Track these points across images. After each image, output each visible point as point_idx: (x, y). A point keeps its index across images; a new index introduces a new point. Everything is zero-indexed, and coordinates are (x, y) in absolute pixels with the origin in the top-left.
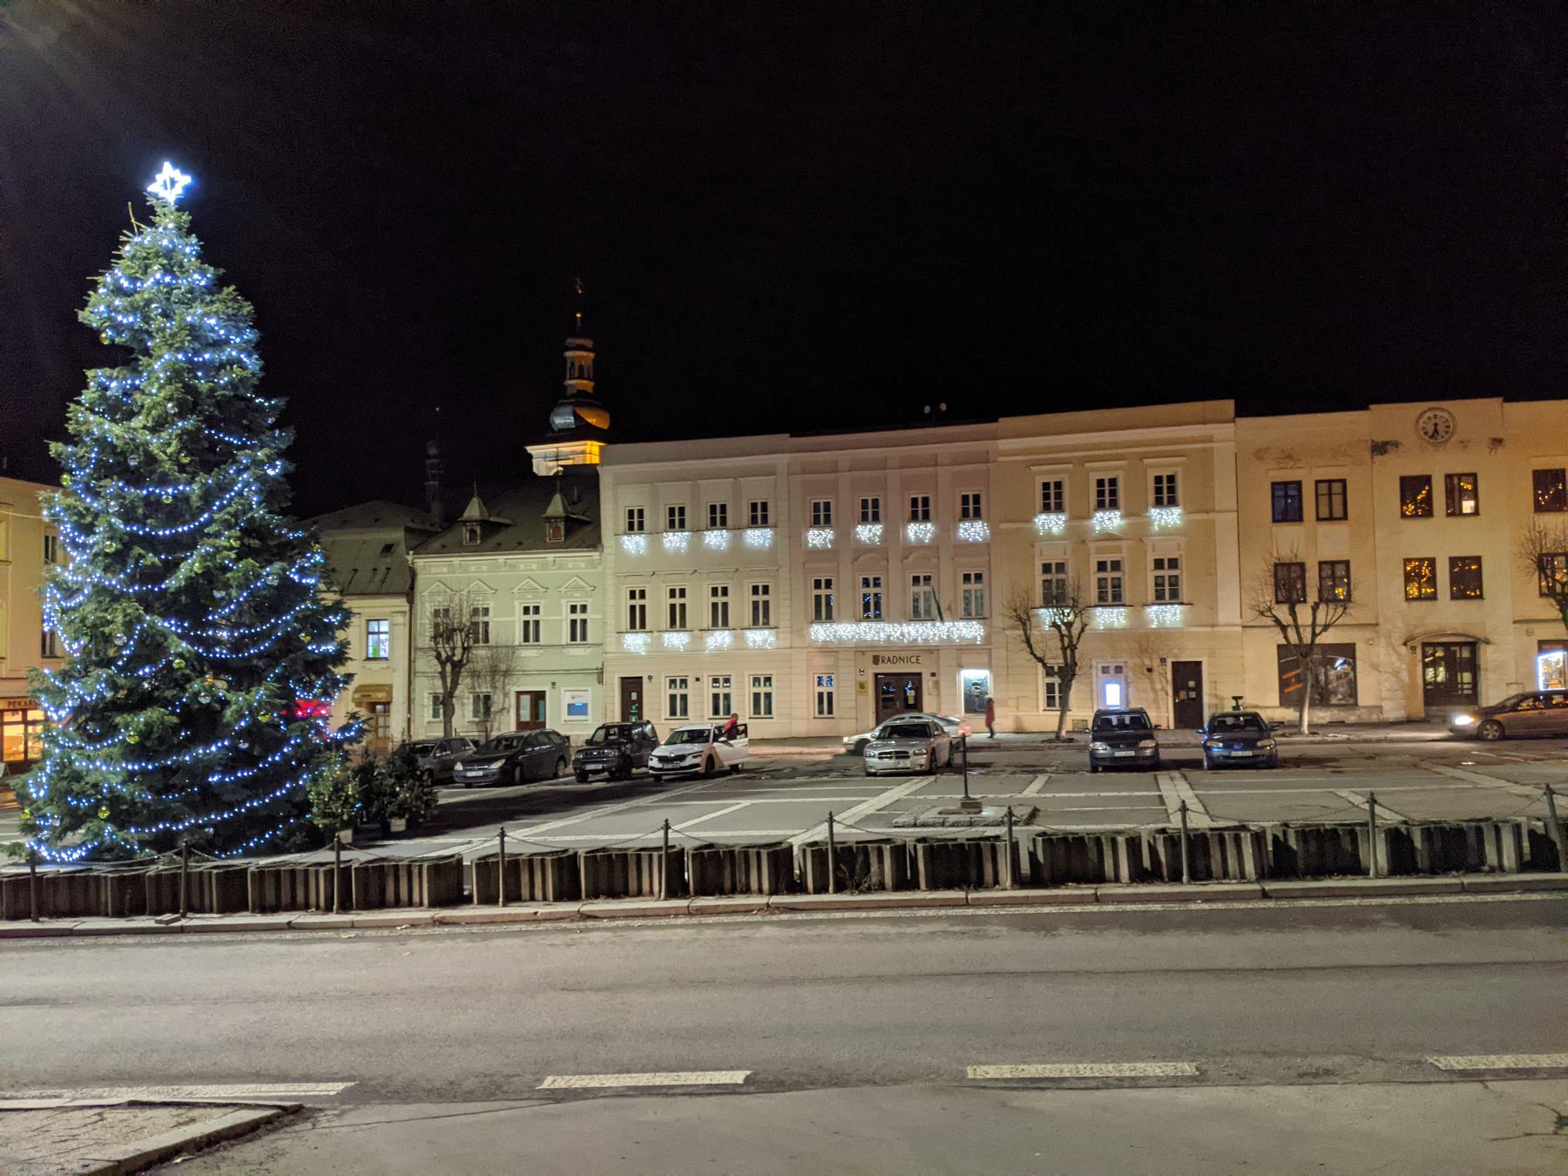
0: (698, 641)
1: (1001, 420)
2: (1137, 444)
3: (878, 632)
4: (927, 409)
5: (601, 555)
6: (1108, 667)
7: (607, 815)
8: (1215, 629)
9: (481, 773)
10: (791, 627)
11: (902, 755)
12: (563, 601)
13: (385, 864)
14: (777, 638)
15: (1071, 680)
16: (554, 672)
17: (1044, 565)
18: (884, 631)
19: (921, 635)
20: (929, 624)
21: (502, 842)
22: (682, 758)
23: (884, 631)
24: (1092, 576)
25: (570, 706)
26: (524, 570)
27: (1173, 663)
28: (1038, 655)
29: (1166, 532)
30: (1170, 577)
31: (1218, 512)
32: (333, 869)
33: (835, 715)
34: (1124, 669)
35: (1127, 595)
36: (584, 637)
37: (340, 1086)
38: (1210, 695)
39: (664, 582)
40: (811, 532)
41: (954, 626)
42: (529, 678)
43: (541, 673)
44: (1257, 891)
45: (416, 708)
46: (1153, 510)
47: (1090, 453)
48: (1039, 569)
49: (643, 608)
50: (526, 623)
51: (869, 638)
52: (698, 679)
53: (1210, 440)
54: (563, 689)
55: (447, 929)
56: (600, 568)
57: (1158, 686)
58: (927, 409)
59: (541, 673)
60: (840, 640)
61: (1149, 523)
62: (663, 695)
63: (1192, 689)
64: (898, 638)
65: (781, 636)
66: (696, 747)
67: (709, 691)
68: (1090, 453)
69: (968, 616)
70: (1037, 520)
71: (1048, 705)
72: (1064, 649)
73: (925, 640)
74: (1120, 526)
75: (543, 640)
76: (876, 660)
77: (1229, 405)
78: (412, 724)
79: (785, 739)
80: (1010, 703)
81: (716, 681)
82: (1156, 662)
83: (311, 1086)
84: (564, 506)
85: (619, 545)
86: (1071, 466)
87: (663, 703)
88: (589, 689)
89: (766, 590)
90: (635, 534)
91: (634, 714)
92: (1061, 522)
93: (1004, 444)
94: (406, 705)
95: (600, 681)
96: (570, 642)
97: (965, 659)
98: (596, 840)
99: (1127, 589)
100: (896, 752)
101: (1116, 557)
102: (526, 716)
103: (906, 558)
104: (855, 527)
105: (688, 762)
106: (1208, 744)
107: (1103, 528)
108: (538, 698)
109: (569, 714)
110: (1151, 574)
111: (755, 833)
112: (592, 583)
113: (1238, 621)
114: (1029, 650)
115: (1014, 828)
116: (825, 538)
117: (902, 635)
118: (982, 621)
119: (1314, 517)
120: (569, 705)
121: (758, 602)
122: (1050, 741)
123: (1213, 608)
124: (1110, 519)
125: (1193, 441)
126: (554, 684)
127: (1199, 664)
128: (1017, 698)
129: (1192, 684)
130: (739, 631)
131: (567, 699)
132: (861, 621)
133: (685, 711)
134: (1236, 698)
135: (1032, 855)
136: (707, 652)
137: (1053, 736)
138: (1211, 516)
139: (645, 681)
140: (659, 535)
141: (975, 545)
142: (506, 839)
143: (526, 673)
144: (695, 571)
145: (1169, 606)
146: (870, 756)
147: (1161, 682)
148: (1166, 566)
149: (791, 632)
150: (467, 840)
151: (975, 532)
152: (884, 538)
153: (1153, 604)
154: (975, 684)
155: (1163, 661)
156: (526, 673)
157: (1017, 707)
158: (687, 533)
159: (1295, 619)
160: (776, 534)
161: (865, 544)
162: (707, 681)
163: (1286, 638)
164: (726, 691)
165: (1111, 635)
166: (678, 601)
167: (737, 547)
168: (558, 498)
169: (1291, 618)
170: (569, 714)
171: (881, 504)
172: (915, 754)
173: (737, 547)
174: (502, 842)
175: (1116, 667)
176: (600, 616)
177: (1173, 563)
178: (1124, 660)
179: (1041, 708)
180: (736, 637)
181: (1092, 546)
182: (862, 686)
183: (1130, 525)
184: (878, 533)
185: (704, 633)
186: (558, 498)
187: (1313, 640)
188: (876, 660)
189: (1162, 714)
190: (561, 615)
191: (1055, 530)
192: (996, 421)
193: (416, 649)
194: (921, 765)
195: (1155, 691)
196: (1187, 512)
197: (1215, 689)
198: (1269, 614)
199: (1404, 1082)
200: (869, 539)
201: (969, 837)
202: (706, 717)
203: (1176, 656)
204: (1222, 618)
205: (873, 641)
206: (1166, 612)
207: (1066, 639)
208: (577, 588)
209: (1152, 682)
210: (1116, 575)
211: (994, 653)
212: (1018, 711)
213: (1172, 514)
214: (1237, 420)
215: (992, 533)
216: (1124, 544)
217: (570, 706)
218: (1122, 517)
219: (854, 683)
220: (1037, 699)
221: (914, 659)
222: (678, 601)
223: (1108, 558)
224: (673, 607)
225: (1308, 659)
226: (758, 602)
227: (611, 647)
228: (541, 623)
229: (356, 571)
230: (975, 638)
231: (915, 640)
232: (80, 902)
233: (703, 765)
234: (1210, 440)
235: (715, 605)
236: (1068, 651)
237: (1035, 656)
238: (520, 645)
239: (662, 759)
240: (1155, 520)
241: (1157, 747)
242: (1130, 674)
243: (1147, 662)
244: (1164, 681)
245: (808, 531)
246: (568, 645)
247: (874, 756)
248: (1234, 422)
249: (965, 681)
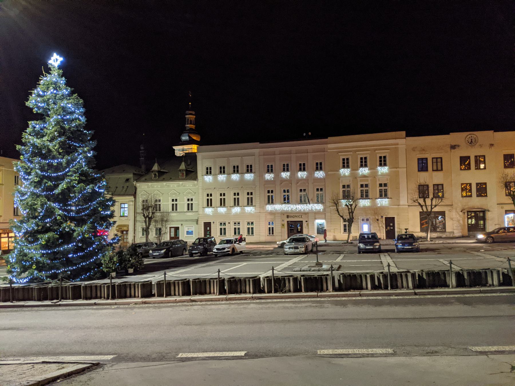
0: (229, 210)
1: (329, 138)
2: (374, 146)
3: (288, 208)
4: (305, 134)
5: (197, 182)
6: (364, 219)
7: (199, 267)
8: (399, 206)
9: (158, 254)
10: (260, 206)
11: (296, 248)
12: (185, 197)
13: (127, 283)
14: (255, 209)
15: (352, 223)
16: (182, 221)
17: (343, 185)
18: (290, 207)
19: (303, 209)
20: (305, 205)
21: (165, 276)
22: (224, 249)
23: (290, 207)
24: (359, 189)
25: (187, 232)
26: (172, 187)
27: (385, 218)
28: (341, 215)
29: (383, 175)
30: (384, 189)
31: (400, 168)
32: (109, 285)
33: (274, 235)
34: (369, 220)
35: (370, 195)
36: (192, 209)
37: (112, 357)
38: (397, 228)
40: (266, 175)
41: (313, 205)
42: (174, 223)
43: (178, 221)
44: (413, 292)
45: (137, 232)
46: (379, 167)
47: (358, 149)
48: (341, 187)
49: (211, 199)
50: (173, 205)
51: (285, 209)
52: (229, 223)
53: (398, 144)
54: (185, 226)
55: (147, 305)
56: (197, 186)
57: (380, 225)
58: (305, 134)
59: (178, 221)
60: (276, 210)
61: (377, 172)
62: (218, 228)
63: (392, 226)
64: (295, 209)
65: (257, 209)
66: (229, 245)
67: (233, 227)
68: (358, 149)
69: (318, 202)
70: (340, 171)
71: (344, 232)
72: (349, 213)
73: (304, 210)
74: (368, 173)
75: (178, 210)
76: (288, 217)
77: (404, 133)
78: (135, 238)
79: (258, 243)
80: (332, 231)
81: (235, 223)
82: (380, 217)
84: (185, 166)
85: (203, 179)
86: (352, 153)
87: (218, 231)
88: (194, 226)
89: (252, 194)
90: (209, 175)
91: (208, 234)
92: (348, 171)
93: (330, 146)
94: (133, 231)
95: (197, 224)
96: (187, 211)
97: (317, 216)
98: (196, 276)
99: (370, 193)
100: (294, 247)
101: (366, 183)
102: (173, 235)
103: (298, 183)
104: (281, 173)
105: (226, 250)
106: (397, 244)
107: (362, 173)
108: (177, 229)
109: (187, 234)
110: (378, 188)
111: (248, 273)
112: (195, 191)
113: (407, 204)
114: (338, 213)
115: (333, 272)
117: (296, 208)
118: (322, 204)
119: (432, 170)
120: (187, 232)
122: (345, 243)
123: (398, 200)
124: (364, 170)
125: (392, 145)
126: (182, 224)
127: (394, 218)
128: (334, 229)
129: (391, 224)
130: (243, 207)
131: (186, 229)
132: (283, 204)
133: (225, 233)
134: (406, 229)
135: (339, 281)
136: (232, 214)
137: (346, 242)
138: (398, 169)
139: (212, 223)
140: (216, 176)
141: (320, 179)
142: (166, 275)
143: (173, 221)
144: (228, 187)
145: (384, 199)
146: (286, 248)
147: (381, 224)
148: (383, 186)
149: (260, 208)
150: (153, 276)
151: (320, 175)
152: (290, 176)
153: (379, 198)
154: (320, 225)
155: (382, 217)
156: (173, 221)
157: (334, 232)
158: (226, 175)
159: (425, 203)
160: (255, 175)
161: (284, 179)
162: (232, 223)
163: (422, 209)
164: (239, 227)
165: (365, 208)
166: (223, 197)
167: (242, 179)
168: (183, 163)
169: (424, 203)
170: (187, 234)
171: (289, 165)
172: (300, 248)
173: (242, 179)
174: (165, 276)
175: (367, 219)
176: (197, 202)
177: (385, 185)
178: (369, 217)
179: (342, 232)
180: (242, 209)
181: (359, 179)
182: (283, 225)
183: (371, 172)
184: (288, 175)
185: (231, 208)
186: (183, 163)
187: (431, 210)
188: (288, 217)
189: (382, 234)
190: (184, 202)
191: (347, 174)
192: (327, 138)
193: (137, 213)
194: (303, 251)
195: (379, 227)
196: (390, 168)
197: (399, 226)
198: (417, 202)
200: (286, 177)
201: (318, 275)
202: (232, 235)
203: (386, 215)
204: (401, 203)
205: (287, 210)
206: (383, 201)
207: (350, 210)
208: (189, 193)
209: (378, 224)
210: (367, 189)
211: (327, 214)
212: (334, 233)
213: (385, 169)
214: (406, 138)
215: (326, 175)
216: (369, 179)
217: (187, 232)
218: (369, 170)
219: (280, 224)
220: (341, 229)
221: (300, 216)
222: (223, 197)
223: (364, 183)
224: (221, 199)
225: (430, 216)
227: (201, 212)
228: (178, 204)
229: (117, 187)
230: (320, 209)
231: (301, 210)
232: (26, 296)
233: (231, 251)
234: (398, 144)
235: (235, 199)
236: (351, 214)
237: (340, 215)
238: (171, 212)
239: (217, 249)
240: (379, 171)
242: (371, 221)
243: (377, 217)
244: (382, 223)
245: (265, 174)
246: (186, 212)
247: (287, 248)
248: (405, 138)
249: (317, 223)
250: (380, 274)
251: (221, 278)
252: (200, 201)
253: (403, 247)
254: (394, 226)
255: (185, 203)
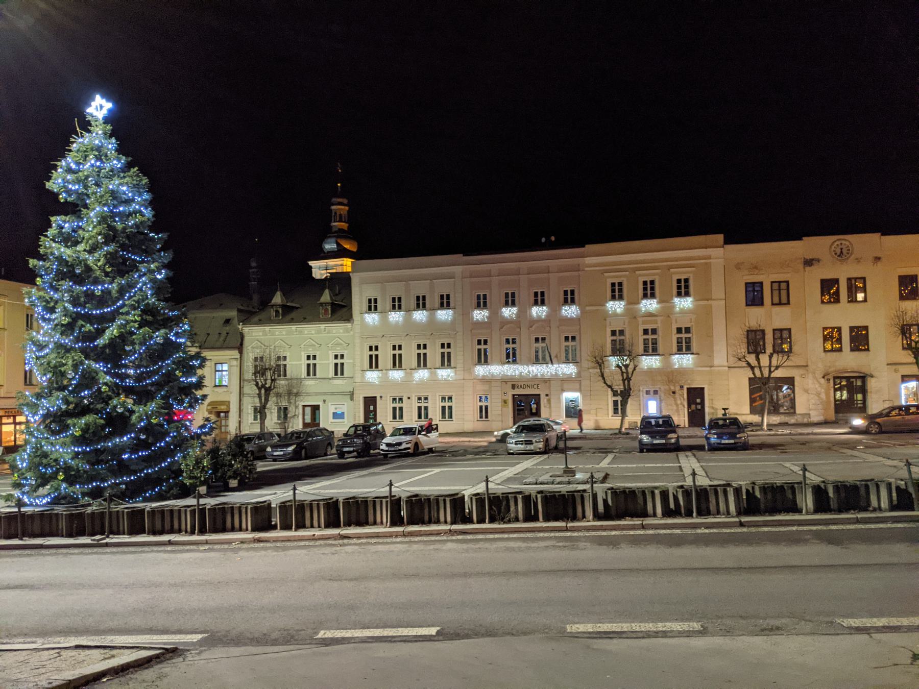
0: (409, 375)
1: (587, 246)
2: (667, 260)
3: (515, 371)
4: (543, 240)
5: (352, 325)
6: (650, 391)
7: (356, 477)
8: (712, 368)
10: (464, 367)
11: (529, 442)
12: (330, 352)
13: (226, 506)
14: (456, 374)
15: (628, 399)
16: (325, 394)
17: (612, 331)
18: (518, 370)
19: (540, 372)
20: (545, 366)
21: (294, 494)
22: (400, 444)
23: (518, 370)
24: (640, 338)
25: (334, 414)
26: (307, 334)
27: (688, 388)
28: (609, 384)
29: (683, 312)
30: (686, 338)
31: (714, 300)
32: (195, 509)
33: (489, 419)
34: (659, 392)
35: (660, 349)
36: (342, 373)
37: (200, 636)
38: (709, 407)
39: (389, 341)
40: (475, 312)
41: (559, 367)
42: (310, 397)
43: (317, 394)
44: (737, 522)
45: (244, 415)
46: (676, 299)
47: (639, 265)
48: (609, 333)
49: (377, 356)
50: (309, 365)
51: (509, 374)
52: (409, 398)
53: (709, 258)
54: (330, 404)
55: (262, 544)
56: (352, 332)
57: (679, 402)
58: (543, 240)
59: (317, 394)
60: (493, 375)
61: (673, 307)
62: (388, 407)
63: (699, 404)
64: (526, 374)
65: (458, 372)
66: (408, 438)
67: (415, 405)
68: (639, 265)
69: (567, 361)
70: (607, 305)
71: (614, 413)
72: (624, 380)
73: (542, 375)
74: (656, 308)
75: (318, 375)
76: (513, 387)
77: (720, 237)
78: (241, 424)
79: (460, 433)
80: (592, 412)
81: (419, 399)
82: (678, 388)
83: (182, 636)
84: (331, 297)
85: (363, 320)
86: (628, 273)
87: (388, 412)
88: (345, 403)
89: (449, 346)
90: (372, 313)
91: (371, 418)
92: (622, 306)
93: (588, 260)
94: (238, 413)
95: (352, 399)
96: (334, 376)
97: (565, 386)
98: (350, 492)
99: (661, 345)
100: (525, 441)
101: (654, 326)
102: (308, 419)
103: (531, 327)
104: (501, 309)
105: (404, 446)
106: (708, 436)
107: (646, 310)
108: (315, 409)
109: (333, 418)
110: (675, 336)
111: (442, 488)
112: (347, 342)
113: (726, 364)
114: (603, 381)
115: (594, 485)
116: (484, 315)
117: (529, 372)
118: (575, 364)
119: (770, 303)
120: (334, 413)
121: (444, 353)
122: (615, 434)
123: (711, 356)
124: (650, 304)
125: (699, 258)
126: (324, 401)
127: (703, 389)
128: (596, 409)
129: (698, 401)
130: (433, 370)
131: (332, 410)
132: (504, 364)
133: (401, 417)
134: (724, 409)
135: (605, 501)
136: (414, 382)
137: (617, 431)
138: (710, 302)
139: (378, 399)
140: (386, 314)
141: (572, 319)
142: (297, 491)
143: (308, 394)
144: (408, 335)
145: (685, 355)
146: (510, 443)
147: (681, 400)
148: (683, 331)
149: (464, 370)
150: (274, 492)
151: (572, 312)
152: (518, 315)
153: (676, 354)
154: (571, 401)
155: (682, 387)
156: (308, 394)
157: (596, 414)
158: (402, 313)
159: (759, 363)
160: (455, 313)
161: (507, 319)
162: (414, 399)
163: (754, 374)
164: (426, 405)
165: (651, 372)
166: (397, 352)
167: (432, 320)
168: (327, 292)
169: (756, 362)
170: (333, 418)
171: (516, 295)
172: (536, 442)
173: (432, 320)
174: (294, 494)
175: (654, 391)
176: (351, 361)
177: (688, 330)
178: (658, 387)
179: (610, 415)
180: (431, 373)
181: (640, 320)
182: (505, 402)
183: (662, 308)
184: (515, 312)
185: (413, 371)
186: (327, 292)
187: (769, 375)
188: (513, 387)
189: (681, 418)
190: (329, 360)
191: (619, 311)
192: (584, 247)
193: (244, 380)
194: (540, 448)
195: (677, 405)
196: (696, 300)
197: (712, 404)
198: (744, 360)
199: (823, 634)
200: (510, 316)
201: (568, 490)
202: (414, 420)
203: (689, 384)
204: (716, 362)
205: (512, 375)
206: (683, 358)
207: (625, 375)
208: (338, 345)
209: (675, 400)
210: (654, 337)
211: (583, 382)
213: (687, 301)
214: (725, 246)
215: (581, 312)
216: (659, 319)
217: (334, 414)
218: (658, 303)
219: (500, 400)
220: (608, 410)
221: (536, 386)
222: (397, 352)
223: (650, 327)
224: (394, 356)
225: (767, 386)
226: (444, 353)
227: (358, 379)
228: (317, 365)
229: (208, 334)
230: (572, 374)
231: (536, 375)
232: (47, 529)
233: (412, 448)
234: (709, 258)
235: (419, 355)
236: (626, 382)
237: (607, 384)
238: (305, 378)
239: (388, 445)
240: (677, 305)
241: (678, 438)
242: (663, 395)
243: (672, 388)
244: (682, 399)
245: (474, 311)
246: (333, 378)
247: (512, 443)
248: (723, 247)
249: (566, 399)
250: (678, 490)
251: (395, 496)
252: (357, 358)
253: (719, 441)
254: (702, 403)
255: (330, 361)
